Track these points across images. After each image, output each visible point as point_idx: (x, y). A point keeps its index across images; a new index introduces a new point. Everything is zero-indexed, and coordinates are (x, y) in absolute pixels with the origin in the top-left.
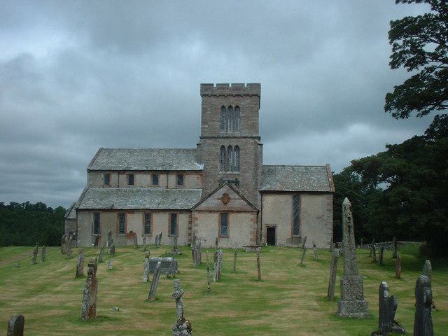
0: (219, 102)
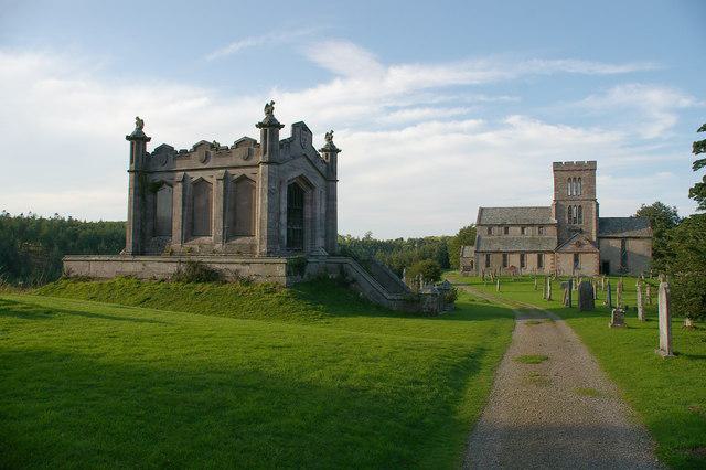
0: (566, 175)
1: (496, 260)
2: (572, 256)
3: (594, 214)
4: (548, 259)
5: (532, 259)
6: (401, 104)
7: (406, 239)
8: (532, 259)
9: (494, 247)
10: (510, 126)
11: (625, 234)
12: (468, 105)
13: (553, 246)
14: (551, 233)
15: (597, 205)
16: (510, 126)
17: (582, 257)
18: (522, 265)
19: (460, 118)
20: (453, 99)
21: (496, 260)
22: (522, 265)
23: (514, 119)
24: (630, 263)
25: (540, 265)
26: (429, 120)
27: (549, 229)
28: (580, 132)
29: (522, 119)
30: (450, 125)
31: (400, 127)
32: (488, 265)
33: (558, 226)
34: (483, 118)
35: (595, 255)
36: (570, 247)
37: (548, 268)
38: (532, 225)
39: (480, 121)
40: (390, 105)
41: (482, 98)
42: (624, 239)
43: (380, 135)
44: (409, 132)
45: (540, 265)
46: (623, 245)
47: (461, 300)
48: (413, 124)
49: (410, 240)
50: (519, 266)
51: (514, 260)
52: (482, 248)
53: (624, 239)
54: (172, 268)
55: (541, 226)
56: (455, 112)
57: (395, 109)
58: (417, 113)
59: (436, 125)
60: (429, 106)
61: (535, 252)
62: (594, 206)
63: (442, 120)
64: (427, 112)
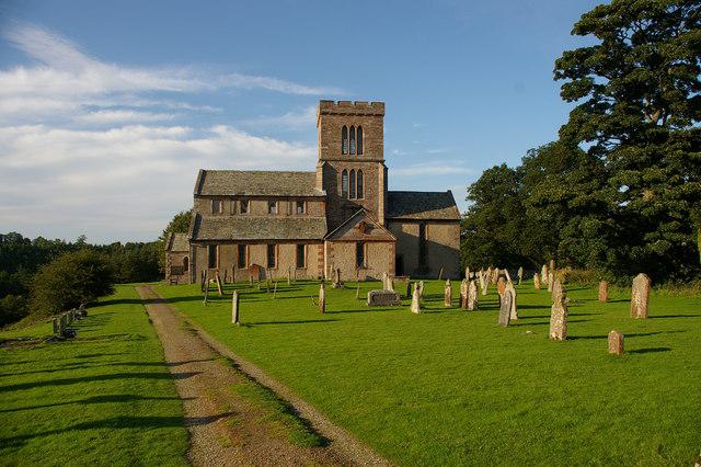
0: (339, 121)
1: (227, 255)
2: (354, 245)
3: (381, 183)
4: (312, 252)
5: (287, 253)
6: (101, 104)
7: (124, 244)
8: (287, 253)
9: (223, 234)
10: (216, 135)
11: (425, 215)
12: (173, 111)
13: (321, 232)
14: (317, 211)
15: (386, 169)
16: (216, 135)
17: (369, 249)
18: (271, 264)
19: (168, 124)
20: (157, 105)
21: (227, 255)
22: (271, 264)
23: (220, 129)
24: (432, 259)
25: (300, 262)
26: (134, 123)
27: (313, 205)
28: (284, 145)
29: (228, 130)
30: (159, 131)
31: (105, 128)
32: (212, 264)
33: (329, 201)
34: (190, 126)
35: (391, 246)
36: (351, 233)
37: (312, 270)
38: (286, 198)
39: (187, 129)
40: (90, 103)
41: (186, 106)
42: (423, 223)
43: (83, 134)
44: (113, 134)
45: (300, 262)
46: (422, 231)
47: (177, 236)
48: (118, 125)
49: (129, 244)
50: (265, 265)
51: (258, 255)
52: (203, 235)
53: (423, 223)
54: (509, 287)
55: (301, 201)
56: (157, 117)
57: (95, 109)
58: (119, 115)
59: (141, 130)
60: (133, 109)
61: (291, 241)
62: (381, 170)
63: (147, 124)
64: (130, 115)
